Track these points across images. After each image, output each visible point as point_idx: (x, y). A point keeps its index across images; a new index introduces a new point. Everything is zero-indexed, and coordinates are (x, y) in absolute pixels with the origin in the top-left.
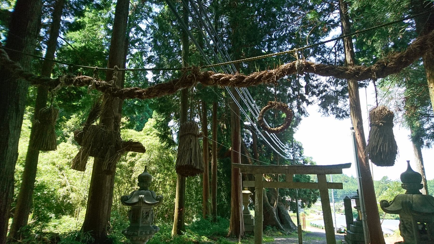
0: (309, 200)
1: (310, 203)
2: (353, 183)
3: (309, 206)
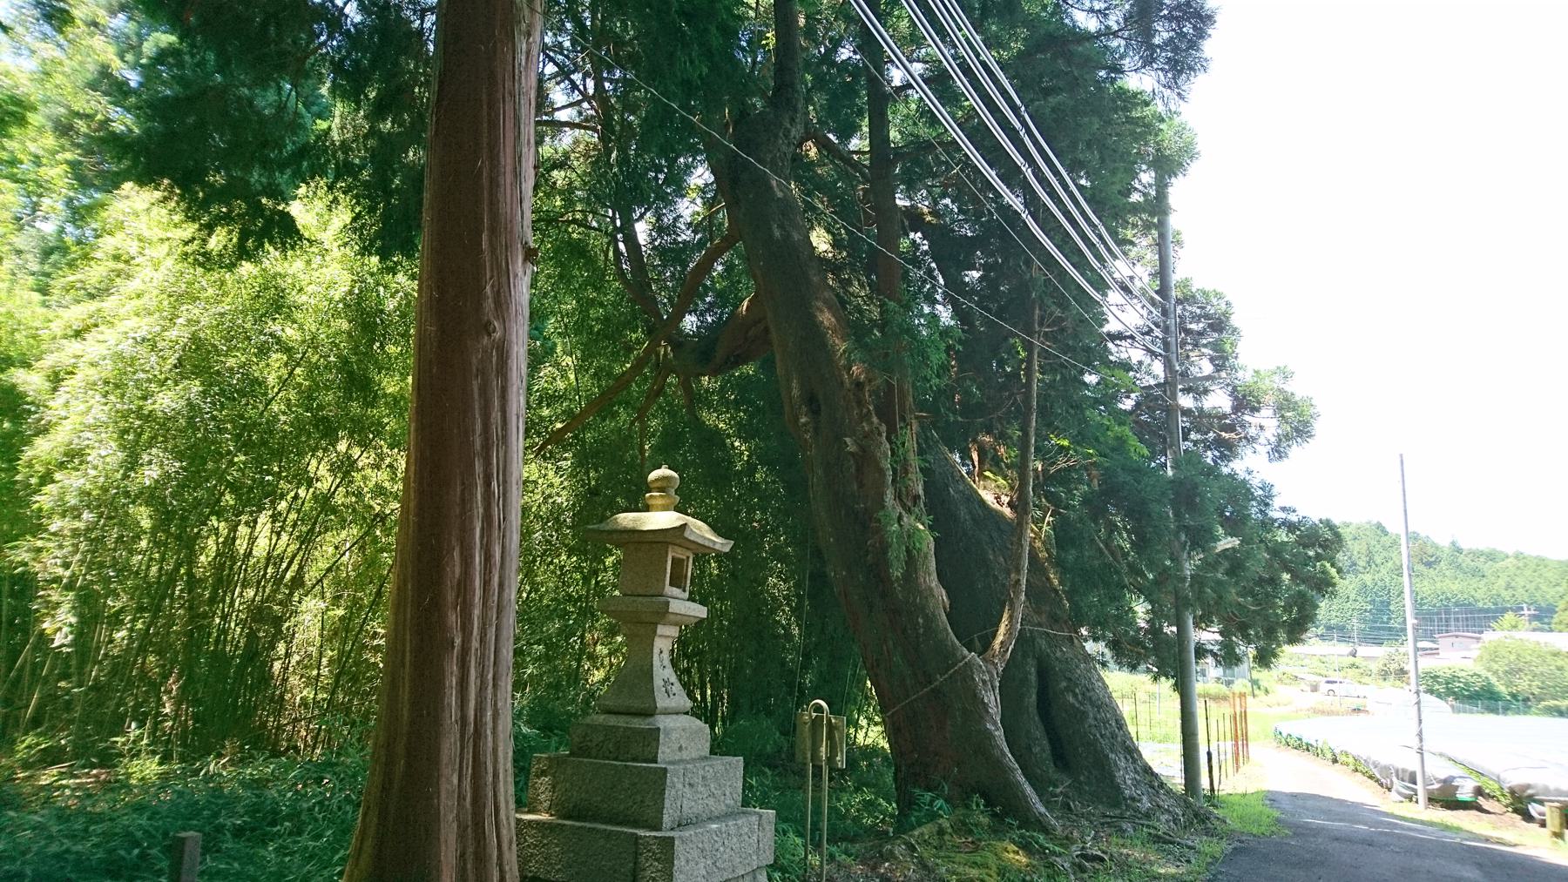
0: (1266, 618)
1: (1270, 633)
2: (1459, 567)
3: (1265, 658)
